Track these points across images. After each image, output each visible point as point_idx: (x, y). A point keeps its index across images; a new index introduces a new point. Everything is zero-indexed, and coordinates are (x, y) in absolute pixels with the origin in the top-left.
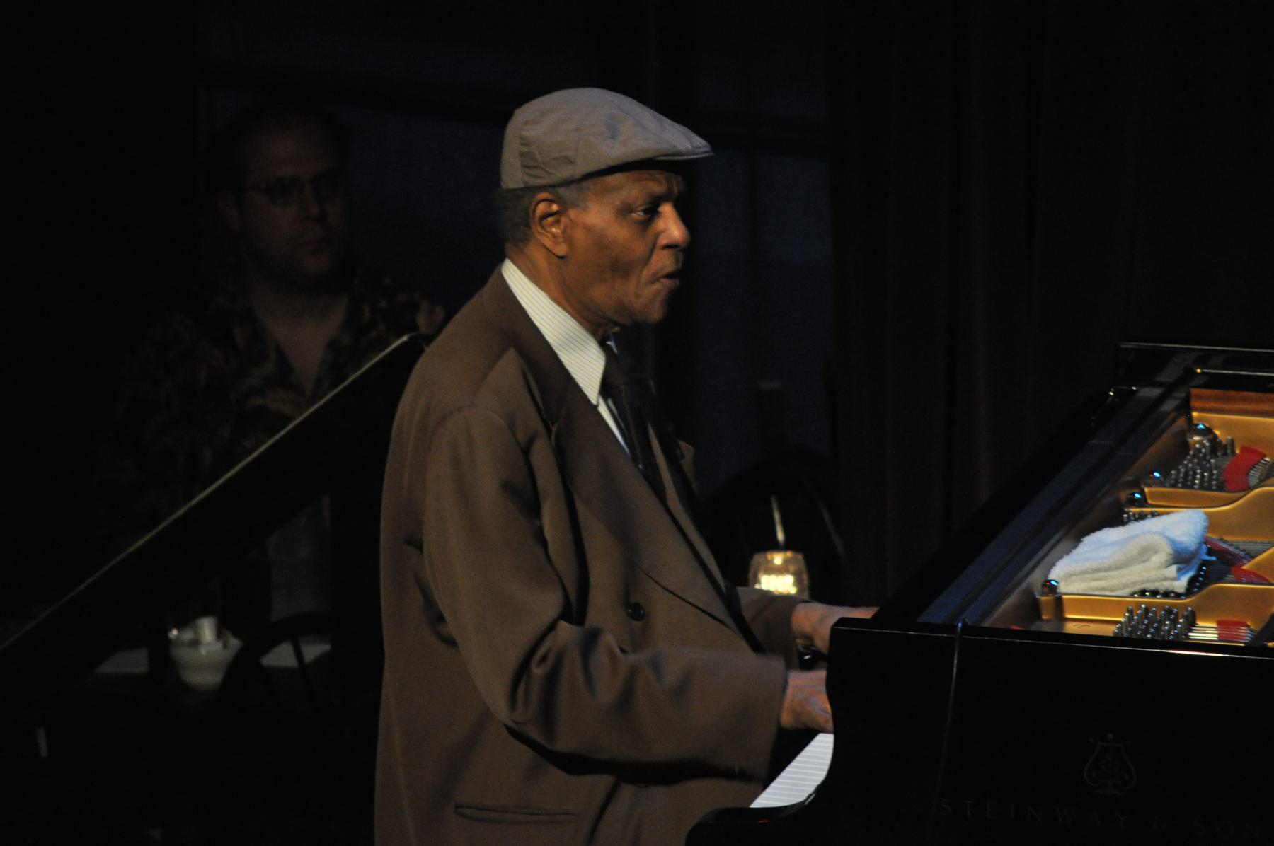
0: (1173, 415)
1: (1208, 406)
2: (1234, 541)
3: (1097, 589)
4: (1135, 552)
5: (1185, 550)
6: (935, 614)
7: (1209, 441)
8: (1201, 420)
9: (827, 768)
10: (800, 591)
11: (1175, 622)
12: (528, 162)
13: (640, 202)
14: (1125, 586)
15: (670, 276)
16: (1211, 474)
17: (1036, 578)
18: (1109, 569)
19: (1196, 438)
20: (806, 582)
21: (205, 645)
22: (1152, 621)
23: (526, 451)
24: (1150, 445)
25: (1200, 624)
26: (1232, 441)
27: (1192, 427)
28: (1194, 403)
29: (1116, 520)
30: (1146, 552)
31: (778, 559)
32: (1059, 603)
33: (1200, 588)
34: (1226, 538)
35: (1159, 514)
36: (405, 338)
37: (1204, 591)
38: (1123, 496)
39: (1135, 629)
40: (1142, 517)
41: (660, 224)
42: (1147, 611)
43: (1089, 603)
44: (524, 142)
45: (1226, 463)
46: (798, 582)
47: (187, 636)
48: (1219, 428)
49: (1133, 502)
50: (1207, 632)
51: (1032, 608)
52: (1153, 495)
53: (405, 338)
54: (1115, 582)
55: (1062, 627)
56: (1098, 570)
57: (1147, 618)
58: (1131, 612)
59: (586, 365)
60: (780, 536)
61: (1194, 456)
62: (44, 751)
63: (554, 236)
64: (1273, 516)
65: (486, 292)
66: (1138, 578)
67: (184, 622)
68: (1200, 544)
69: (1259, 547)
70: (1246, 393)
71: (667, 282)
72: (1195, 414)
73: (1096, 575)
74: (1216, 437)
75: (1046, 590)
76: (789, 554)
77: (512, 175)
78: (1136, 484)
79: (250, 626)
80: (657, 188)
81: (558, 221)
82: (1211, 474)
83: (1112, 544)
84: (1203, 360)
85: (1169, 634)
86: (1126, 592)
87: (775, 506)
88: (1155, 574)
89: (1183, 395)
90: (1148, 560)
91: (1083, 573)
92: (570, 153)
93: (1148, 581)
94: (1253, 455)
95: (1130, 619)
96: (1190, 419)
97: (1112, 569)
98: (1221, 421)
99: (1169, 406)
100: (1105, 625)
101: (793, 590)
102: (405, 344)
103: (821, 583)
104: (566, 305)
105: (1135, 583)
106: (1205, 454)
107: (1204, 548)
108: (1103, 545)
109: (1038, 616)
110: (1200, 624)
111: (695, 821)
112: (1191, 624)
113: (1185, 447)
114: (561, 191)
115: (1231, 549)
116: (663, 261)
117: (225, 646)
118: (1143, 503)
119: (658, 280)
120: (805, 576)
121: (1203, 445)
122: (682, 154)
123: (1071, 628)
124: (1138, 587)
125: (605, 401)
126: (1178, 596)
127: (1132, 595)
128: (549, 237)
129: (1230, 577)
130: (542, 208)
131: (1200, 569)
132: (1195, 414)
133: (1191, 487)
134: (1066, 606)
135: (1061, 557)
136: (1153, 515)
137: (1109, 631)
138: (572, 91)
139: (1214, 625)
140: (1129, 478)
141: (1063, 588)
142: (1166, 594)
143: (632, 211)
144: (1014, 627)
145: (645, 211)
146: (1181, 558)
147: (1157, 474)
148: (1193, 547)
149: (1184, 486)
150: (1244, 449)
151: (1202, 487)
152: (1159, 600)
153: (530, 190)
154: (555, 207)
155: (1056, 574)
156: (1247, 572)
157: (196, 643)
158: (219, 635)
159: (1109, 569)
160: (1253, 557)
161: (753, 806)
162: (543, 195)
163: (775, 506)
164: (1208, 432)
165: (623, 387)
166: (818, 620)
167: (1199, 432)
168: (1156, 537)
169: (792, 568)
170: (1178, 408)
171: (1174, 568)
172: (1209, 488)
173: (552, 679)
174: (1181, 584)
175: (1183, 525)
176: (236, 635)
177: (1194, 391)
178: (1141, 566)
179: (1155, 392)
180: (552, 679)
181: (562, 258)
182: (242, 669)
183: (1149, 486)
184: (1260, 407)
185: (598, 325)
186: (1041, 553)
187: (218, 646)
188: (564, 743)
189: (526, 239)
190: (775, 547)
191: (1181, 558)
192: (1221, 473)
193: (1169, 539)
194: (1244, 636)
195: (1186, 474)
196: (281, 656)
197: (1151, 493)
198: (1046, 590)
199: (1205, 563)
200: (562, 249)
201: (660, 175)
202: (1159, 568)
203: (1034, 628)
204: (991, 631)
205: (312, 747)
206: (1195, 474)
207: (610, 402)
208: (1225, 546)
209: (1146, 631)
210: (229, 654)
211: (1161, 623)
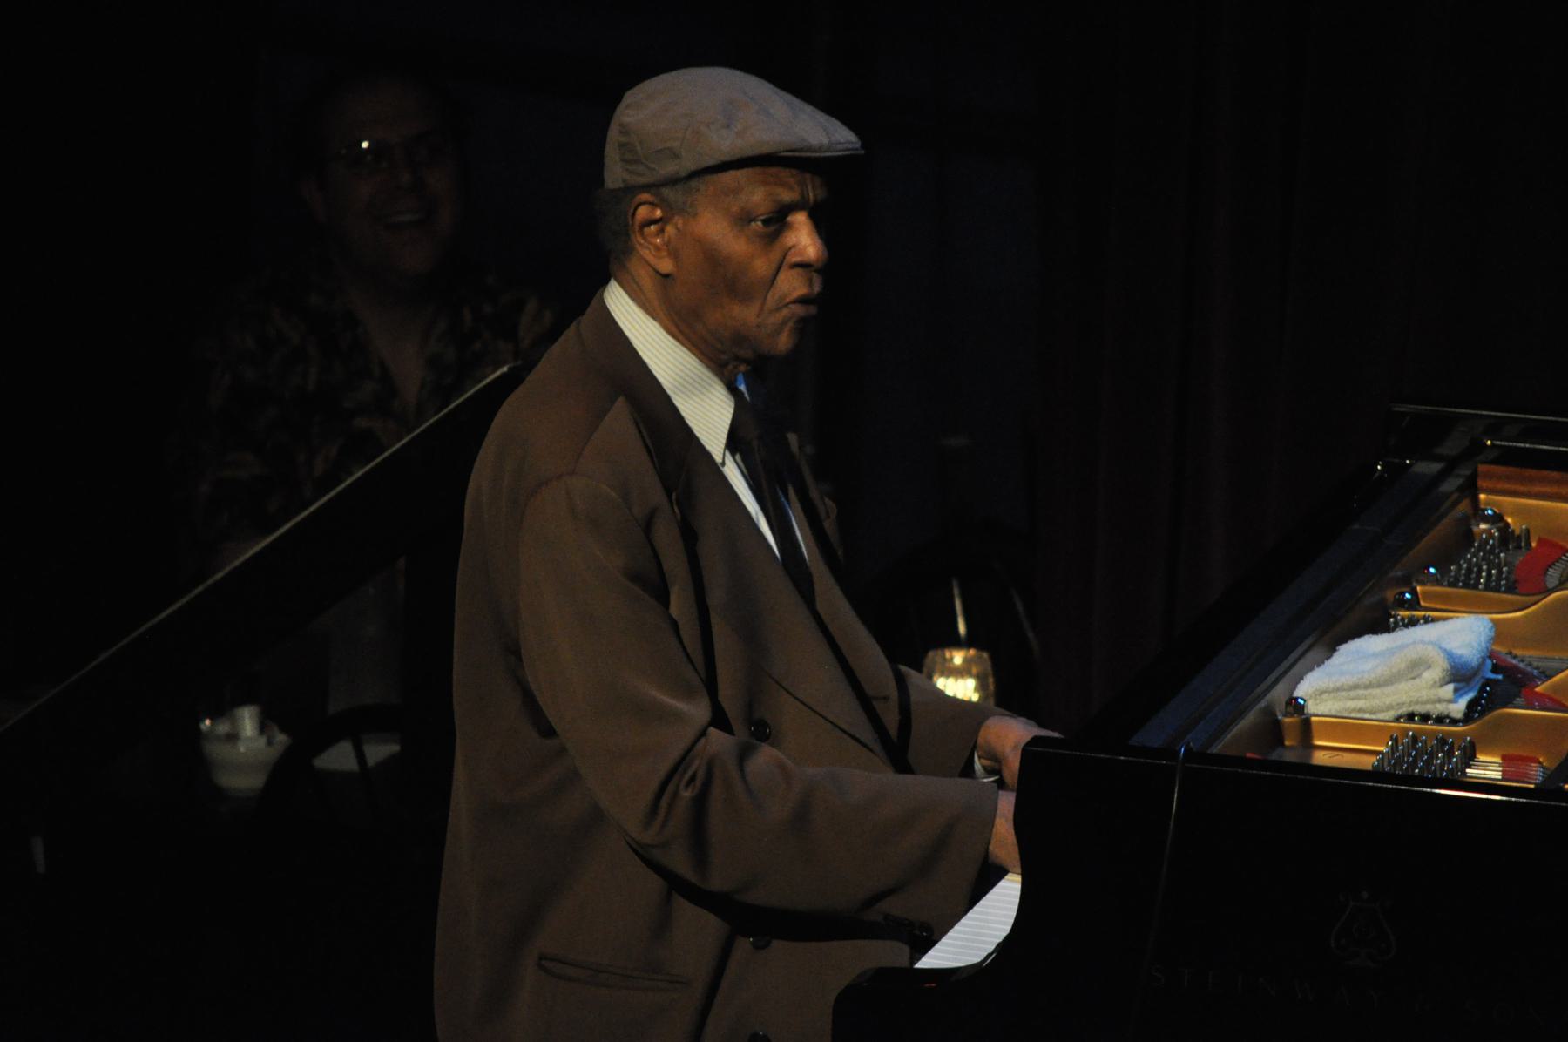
0: (1456, 495)
1: (1499, 486)
2: (1527, 656)
3: (1354, 710)
4: (1403, 666)
5: (1464, 666)
6: (1151, 735)
7: (1499, 530)
8: (1488, 503)
9: (1012, 921)
10: (983, 698)
11: (1450, 754)
12: (631, 157)
13: (762, 210)
14: (1389, 708)
15: (803, 301)
16: (1500, 572)
17: (1278, 694)
18: (1367, 687)
19: (1483, 526)
20: (992, 687)
21: (245, 740)
22: (1420, 753)
23: (648, 526)
24: (1422, 537)
25: (1481, 758)
26: (1528, 531)
27: (1478, 513)
28: (1481, 483)
29: (1380, 624)
30: (1416, 667)
31: (958, 658)
32: (1306, 726)
33: (1482, 713)
34: (1516, 652)
35: (1434, 620)
36: (505, 369)
37: (1486, 718)
38: (1390, 595)
39: (1399, 762)
40: (1413, 622)
41: (790, 238)
42: (1415, 739)
43: (1343, 728)
44: (625, 130)
45: (1520, 558)
46: (981, 687)
47: (223, 728)
48: (1512, 515)
49: (1402, 604)
50: (1488, 768)
51: (1272, 731)
52: (1427, 596)
53: (505, 369)
54: (1376, 702)
55: (1310, 756)
56: (1356, 687)
57: (1414, 748)
58: (1396, 741)
59: (709, 413)
60: (962, 628)
61: (1480, 549)
62: (41, 867)
63: (658, 249)
64: (1567, 627)
65: (586, 318)
66: (1405, 698)
67: (220, 710)
68: (1484, 660)
69: (1556, 665)
70: (1546, 473)
71: (800, 310)
72: (1482, 496)
73: (1353, 693)
74: (1507, 525)
75: (1290, 709)
76: (972, 652)
77: (615, 174)
78: (1407, 581)
79: (302, 721)
80: (787, 196)
81: (662, 231)
82: (1500, 572)
83: (1375, 655)
84: (1494, 429)
85: (1442, 770)
86: (1391, 714)
87: (956, 591)
88: (1426, 694)
89: (1468, 473)
90: (1419, 676)
91: (1338, 690)
92: (676, 144)
93: (1417, 703)
94: (1552, 550)
95: (1394, 748)
96: (1476, 500)
97: (1374, 685)
98: (1515, 506)
99: (1450, 485)
100: (1362, 755)
101: (975, 697)
102: (504, 375)
103: (1007, 691)
104: (674, 329)
105: (1400, 705)
106: (1493, 547)
107: (1489, 664)
108: (1363, 657)
109: (1280, 742)
110: (1481, 758)
111: (845, 983)
112: (1469, 758)
113: (1469, 536)
114: (666, 192)
115: (1521, 665)
116: (792, 285)
117: (270, 743)
118: (1414, 604)
119: (786, 305)
120: (991, 680)
121: (1491, 536)
122: (810, 149)
123: (1320, 758)
124: (1405, 710)
125: (733, 456)
126: (1454, 722)
127: (1397, 719)
128: (651, 252)
129: (1519, 700)
130: (643, 212)
131: (1482, 690)
132: (1482, 496)
133: (1475, 587)
135: (1311, 669)
136: (1427, 620)
137: (1368, 763)
138: (738, 73)
139: (1498, 760)
140: (1398, 572)
141: (1311, 708)
142: (1440, 720)
143: (754, 220)
144: (1249, 755)
145: (766, 222)
146: (1459, 675)
147: (1432, 570)
148: (1475, 663)
149: (1466, 586)
150: (1541, 542)
151: (1487, 588)
152: (1430, 726)
153: (630, 190)
154: (658, 213)
155: (1302, 690)
156: (1541, 695)
157: (233, 737)
158: (262, 728)
160: (1551, 677)
161: (918, 966)
162: (645, 196)
163: (956, 591)
164: (1498, 518)
165: (755, 443)
166: (1011, 735)
167: (1486, 519)
168: (1430, 648)
169: (974, 670)
170: (1461, 489)
171: (1451, 687)
172: (1497, 589)
173: (700, 803)
174: (1458, 708)
175: (1464, 634)
176: (283, 730)
177: (1481, 468)
179: (1435, 467)
180: (700, 803)
181: (666, 276)
182: (289, 772)
183: (1423, 583)
184: (1537, 489)
185: (723, 356)
186: (1286, 664)
187: (263, 741)
188: (717, 882)
189: (628, 250)
190: (957, 643)
191: (1459, 675)
192: (1508, 570)
193: (1445, 651)
194: (1535, 776)
195: (1469, 570)
196: (339, 758)
197: (1424, 593)
198: (1290, 709)
199: (1488, 682)
200: (666, 266)
201: (785, 173)
202: (1434, 685)
203: (1274, 756)
204: (1221, 759)
205: (361, 871)
206: (1480, 571)
207: (738, 457)
208: (1514, 662)
209: (1414, 764)
210: (274, 753)
211: (1432, 755)
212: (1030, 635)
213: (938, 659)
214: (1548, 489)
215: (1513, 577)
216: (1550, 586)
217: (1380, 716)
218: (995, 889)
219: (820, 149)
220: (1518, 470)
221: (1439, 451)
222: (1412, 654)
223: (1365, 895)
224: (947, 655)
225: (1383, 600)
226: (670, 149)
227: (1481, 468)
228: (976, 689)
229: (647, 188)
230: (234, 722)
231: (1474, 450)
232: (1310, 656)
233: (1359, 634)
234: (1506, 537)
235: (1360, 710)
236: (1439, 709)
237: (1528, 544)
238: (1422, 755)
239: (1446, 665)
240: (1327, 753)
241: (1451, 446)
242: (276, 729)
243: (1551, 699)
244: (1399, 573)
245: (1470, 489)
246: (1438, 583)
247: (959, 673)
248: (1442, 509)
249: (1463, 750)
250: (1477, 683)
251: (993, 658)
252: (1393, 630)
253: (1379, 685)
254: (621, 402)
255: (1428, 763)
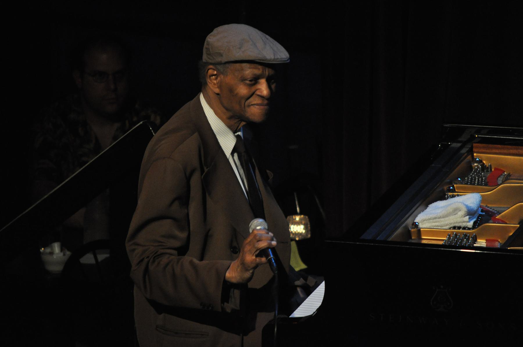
0: (466, 154)
1: (480, 151)
2: (492, 207)
3: (435, 226)
4: (451, 211)
6: (368, 235)
7: (481, 165)
8: (477, 156)
11: (468, 239)
13: (249, 77)
16: (482, 179)
17: (409, 221)
18: (440, 218)
19: (475, 164)
20: (309, 228)
21: (56, 254)
26: (491, 165)
27: (474, 160)
28: (474, 150)
29: (443, 197)
30: (456, 211)
31: (297, 218)
32: (419, 231)
33: (479, 225)
34: (488, 206)
35: (460, 195)
36: (141, 123)
37: (480, 227)
38: (446, 188)
40: (453, 196)
42: (456, 235)
46: (306, 228)
47: (48, 250)
48: (485, 160)
49: (449, 191)
51: (408, 233)
52: (458, 188)
53: (141, 123)
54: (442, 223)
56: (435, 218)
57: (456, 238)
58: (450, 236)
60: (298, 210)
61: (475, 172)
66: (452, 221)
68: (478, 209)
69: (503, 209)
72: (475, 154)
73: (434, 220)
74: (484, 164)
75: (414, 226)
76: (302, 216)
78: (451, 183)
83: (441, 207)
84: (478, 131)
86: (448, 227)
88: (459, 220)
90: (457, 214)
91: (429, 219)
95: (449, 238)
96: (473, 156)
98: (486, 157)
99: (464, 151)
107: (480, 209)
112: (475, 241)
113: (471, 168)
115: (491, 210)
117: (64, 255)
118: (454, 191)
120: (309, 225)
121: (479, 167)
122: (266, 60)
123: (424, 242)
124: (452, 225)
126: (469, 229)
127: (450, 228)
129: (491, 221)
131: (478, 218)
132: (475, 154)
133: (474, 184)
134: (422, 233)
136: (458, 195)
137: (441, 243)
141: (421, 226)
142: (464, 228)
146: (470, 213)
148: (475, 209)
150: (495, 169)
151: (478, 184)
155: (417, 220)
156: (498, 219)
157: (52, 253)
158: (62, 250)
159: (440, 218)
160: (500, 214)
164: (480, 161)
167: (477, 162)
169: (303, 222)
170: (467, 152)
171: (468, 217)
172: (481, 185)
174: (470, 224)
175: (471, 199)
176: (68, 250)
177: (474, 145)
178: (454, 217)
179: (459, 145)
181: (218, 94)
182: (71, 264)
183: (456, 184)
184: (494, 151)
185: (234, 119)
187: (62, 254)
190: (296, 214)
191: (470, 213)
192: (484, 178)
195: (472, 179)
196: (88, 259)
198: (414, 226)
199: (480, 215)
200: (217, 90)
202: (462, 217)
204: (392, 242)
206: (475, 179)
210: (66, 258)
211: (462, 240)
212: (321, 210)
213: (291, 219)
214: (497, 151)
215: (486, 181)
216: (499, 183)
217: (444, 228)
218: (317, 289)
219: (270, 60)
220: (487, 145)
221: (460, 139)
222: (454, 206)
223: (442, 287)
224: (294, 217)
225: (443, 190)
226: (220, 53)
227: (474, 145)
228: (304, 229)
229: (211, 64)
230: (52, 249)
231: (472, 139)
232: (419, 209)
233: (436, 201)
234: (484, 168)
235: (437, 226)
236: (464, 225)
237: (491, 170)
238: (458, 238)
239: (466, 210)
240: (426, 239)
241: (464, 137)
242: (66, 250)
243: (500, 220)
244: (448, 181)
245: (471, 152)
246: (462, 183)
247: (298, 223)
248: (462, 159)
249: (473, 238)
250: (476, 215)
251: (309, 218)
252: (447, 199)
253: (443, 218)
254: (196, 134)
255: (461, 243)
